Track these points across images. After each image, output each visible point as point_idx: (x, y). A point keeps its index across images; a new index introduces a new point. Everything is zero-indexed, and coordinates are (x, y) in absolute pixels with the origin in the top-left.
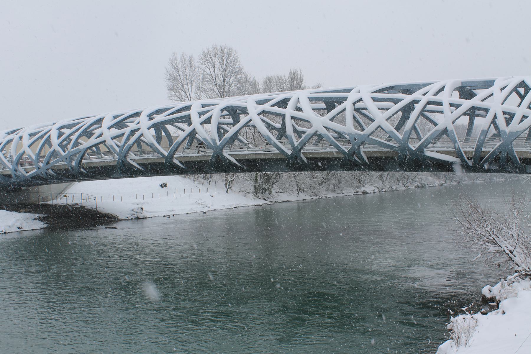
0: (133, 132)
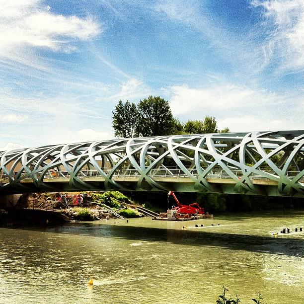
0: (83, 158)
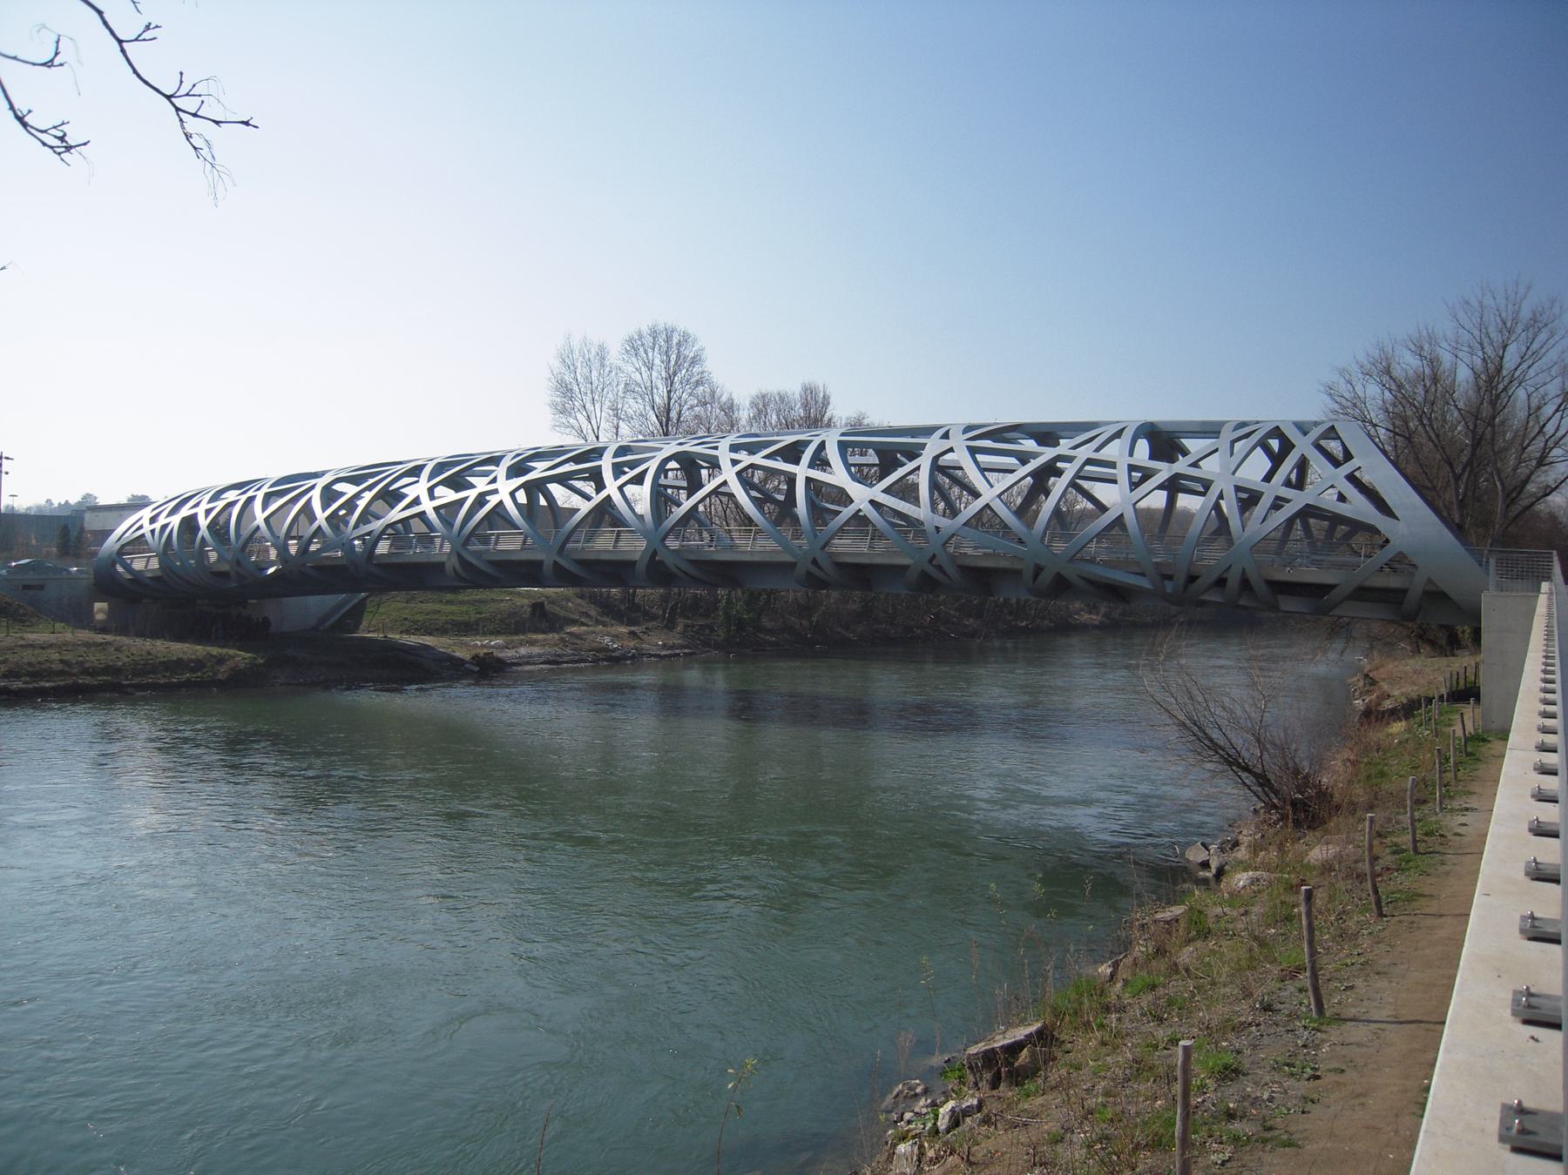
0: (481, 500)
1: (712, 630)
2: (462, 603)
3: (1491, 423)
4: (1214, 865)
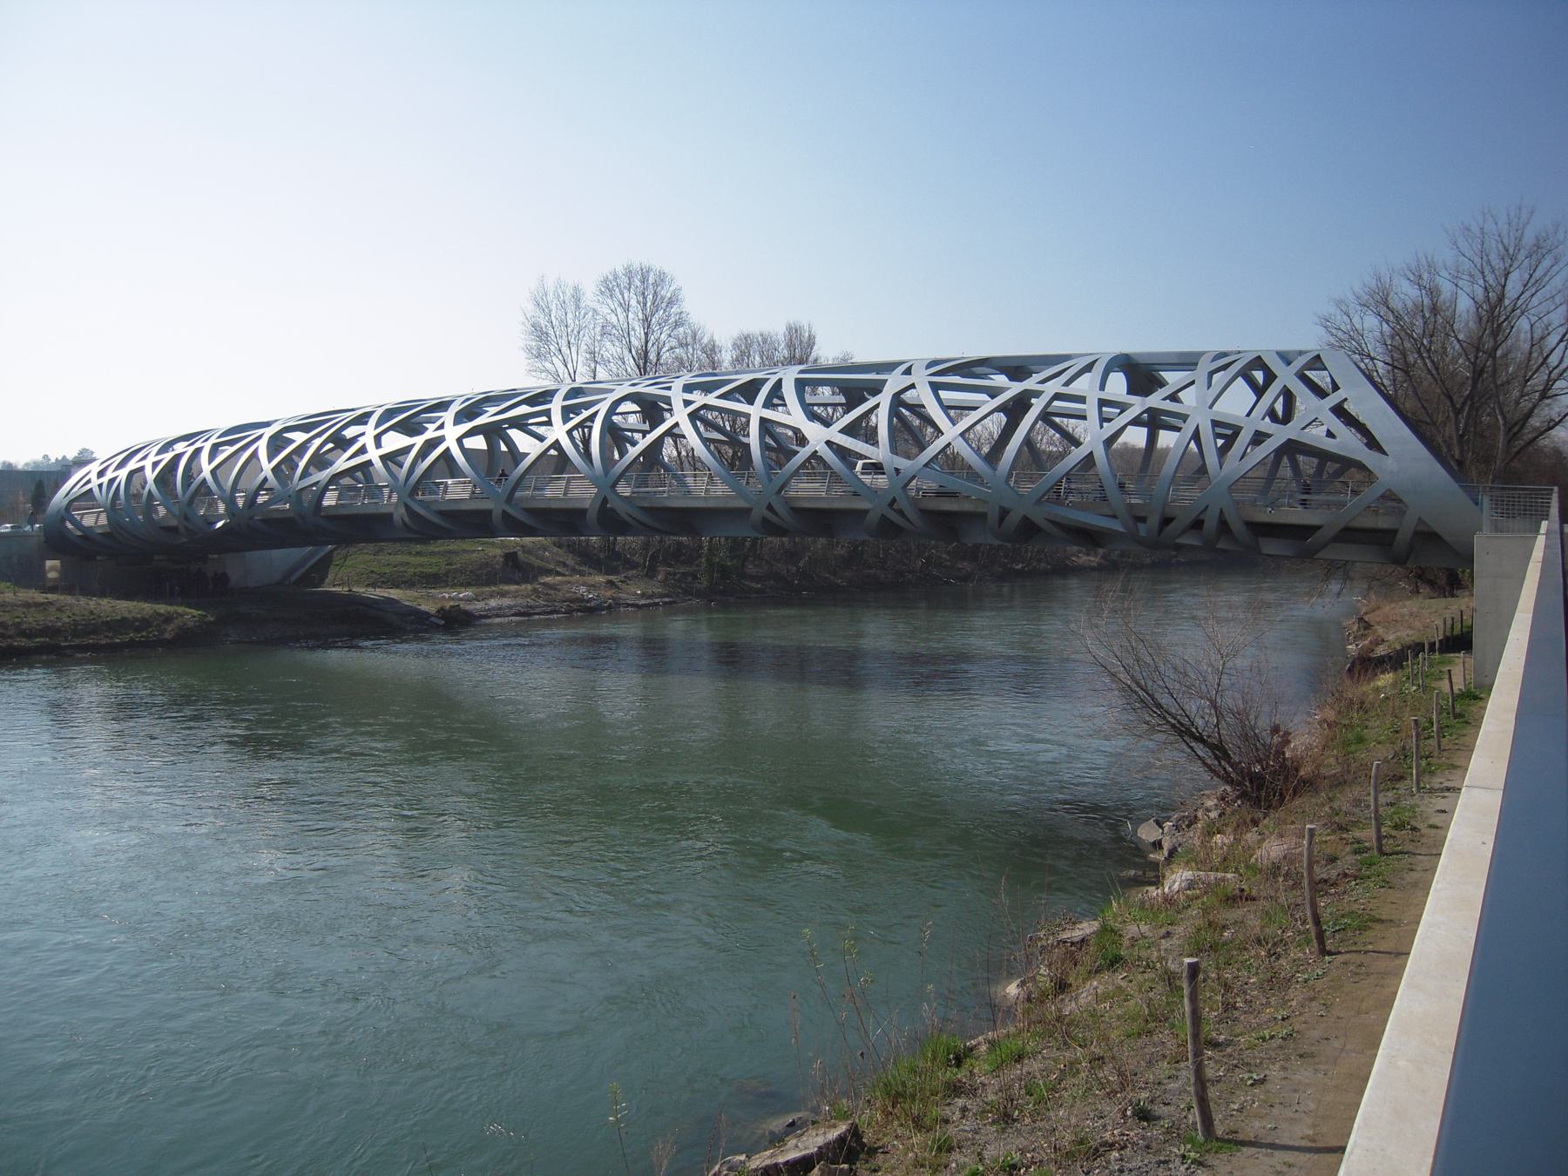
0: (431, 444)
1: (695, 577)
2: (432, 554)
3: (1492, 354)
4: (1166, 846)
